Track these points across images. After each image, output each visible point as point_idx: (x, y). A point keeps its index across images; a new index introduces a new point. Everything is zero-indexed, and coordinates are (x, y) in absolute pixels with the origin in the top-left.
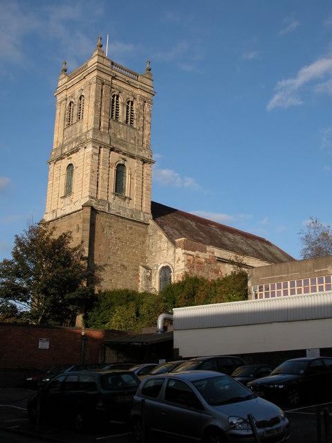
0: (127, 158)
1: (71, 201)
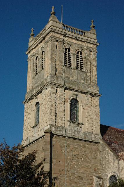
1: (39, 129)
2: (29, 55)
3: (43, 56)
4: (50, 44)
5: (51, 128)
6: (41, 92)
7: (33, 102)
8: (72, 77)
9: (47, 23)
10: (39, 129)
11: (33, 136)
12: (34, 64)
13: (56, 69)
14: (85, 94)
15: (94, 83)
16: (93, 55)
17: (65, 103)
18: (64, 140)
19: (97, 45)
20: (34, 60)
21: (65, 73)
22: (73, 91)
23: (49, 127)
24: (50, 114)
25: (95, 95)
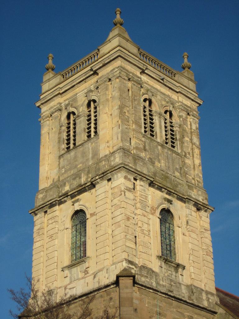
0: (175, 201)
1: (86, 272)
7: (66, 211)
8: (159, 162)
9: (103, 40)
11: (69, 287)
12: (61, 127)
14: (185, 202)
15: (197, 181)
16: (193, 123)
18: (154, 299)
19: (200, 105)
22: (163, 192)
23: (125, 265)
24: (126, 236)
25: (202, 207)
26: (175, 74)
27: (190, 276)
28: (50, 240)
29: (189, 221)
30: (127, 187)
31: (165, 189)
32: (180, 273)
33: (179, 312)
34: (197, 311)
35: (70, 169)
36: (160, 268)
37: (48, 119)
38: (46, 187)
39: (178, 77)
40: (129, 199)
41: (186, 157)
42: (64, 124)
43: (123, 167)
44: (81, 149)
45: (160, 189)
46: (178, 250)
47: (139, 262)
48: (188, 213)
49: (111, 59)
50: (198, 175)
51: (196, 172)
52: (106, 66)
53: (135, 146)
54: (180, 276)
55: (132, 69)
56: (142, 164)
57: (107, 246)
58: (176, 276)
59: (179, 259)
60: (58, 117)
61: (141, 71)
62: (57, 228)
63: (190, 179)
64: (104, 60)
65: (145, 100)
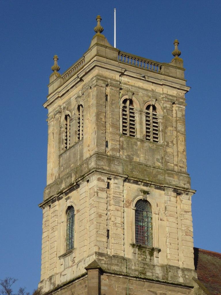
1: (73, 261)
2: (50, 109)
3: (81, 113)
4: (93, 92)
5: (100, 259)
6: (78, 186)
7: (61, 206)
10: (73, 261)
12: (61, 128)
13: (107, 142)
14: (164, 190)
16: (178, 111)
17: (126, 209)
19: (187, 91)
20: (62, 120)
21: (123, 149)
22: (139, 185)
23: (94, 257)
24: (97, 232)
25: (183, 192)
26: (161, 66)
27: (167, 256)
28: (52, 231)
29: (167, 207)
30: (99, 188)
31: (142, 182)
32: (155, 256)
33: (151, 291)
34: (171, 288)
35: (66, 168)
36: (134, 254)
37: (53, 119)
38: (51, 183)
39: (164, 69)
40: (102, 198)
41: (169, 147)
42: (63, 126)
43: (96, 171)
44: (73, 150)
45: (136, 182)
46: (154, 235)
47: (111, 252)
48: (166, 199)
49: (91, 68)
50: (181, 160)
51: (179, 158)
52: (88, 74)
53: (111, 148)
54: (155, 259)
55: (110, 74)
56: (117, 164)
57: (86, 240)
58: (150, 259)
59: (155, 243)
60: (59, 119)
61: (120, 74)
62: (56, 221)
63: (171, 166)
64: (86, 69)
65: (125, 102)
